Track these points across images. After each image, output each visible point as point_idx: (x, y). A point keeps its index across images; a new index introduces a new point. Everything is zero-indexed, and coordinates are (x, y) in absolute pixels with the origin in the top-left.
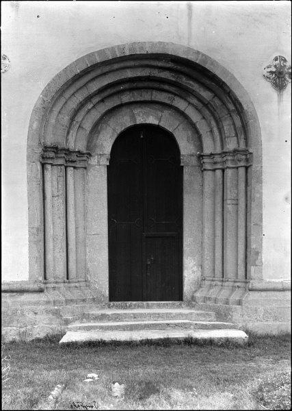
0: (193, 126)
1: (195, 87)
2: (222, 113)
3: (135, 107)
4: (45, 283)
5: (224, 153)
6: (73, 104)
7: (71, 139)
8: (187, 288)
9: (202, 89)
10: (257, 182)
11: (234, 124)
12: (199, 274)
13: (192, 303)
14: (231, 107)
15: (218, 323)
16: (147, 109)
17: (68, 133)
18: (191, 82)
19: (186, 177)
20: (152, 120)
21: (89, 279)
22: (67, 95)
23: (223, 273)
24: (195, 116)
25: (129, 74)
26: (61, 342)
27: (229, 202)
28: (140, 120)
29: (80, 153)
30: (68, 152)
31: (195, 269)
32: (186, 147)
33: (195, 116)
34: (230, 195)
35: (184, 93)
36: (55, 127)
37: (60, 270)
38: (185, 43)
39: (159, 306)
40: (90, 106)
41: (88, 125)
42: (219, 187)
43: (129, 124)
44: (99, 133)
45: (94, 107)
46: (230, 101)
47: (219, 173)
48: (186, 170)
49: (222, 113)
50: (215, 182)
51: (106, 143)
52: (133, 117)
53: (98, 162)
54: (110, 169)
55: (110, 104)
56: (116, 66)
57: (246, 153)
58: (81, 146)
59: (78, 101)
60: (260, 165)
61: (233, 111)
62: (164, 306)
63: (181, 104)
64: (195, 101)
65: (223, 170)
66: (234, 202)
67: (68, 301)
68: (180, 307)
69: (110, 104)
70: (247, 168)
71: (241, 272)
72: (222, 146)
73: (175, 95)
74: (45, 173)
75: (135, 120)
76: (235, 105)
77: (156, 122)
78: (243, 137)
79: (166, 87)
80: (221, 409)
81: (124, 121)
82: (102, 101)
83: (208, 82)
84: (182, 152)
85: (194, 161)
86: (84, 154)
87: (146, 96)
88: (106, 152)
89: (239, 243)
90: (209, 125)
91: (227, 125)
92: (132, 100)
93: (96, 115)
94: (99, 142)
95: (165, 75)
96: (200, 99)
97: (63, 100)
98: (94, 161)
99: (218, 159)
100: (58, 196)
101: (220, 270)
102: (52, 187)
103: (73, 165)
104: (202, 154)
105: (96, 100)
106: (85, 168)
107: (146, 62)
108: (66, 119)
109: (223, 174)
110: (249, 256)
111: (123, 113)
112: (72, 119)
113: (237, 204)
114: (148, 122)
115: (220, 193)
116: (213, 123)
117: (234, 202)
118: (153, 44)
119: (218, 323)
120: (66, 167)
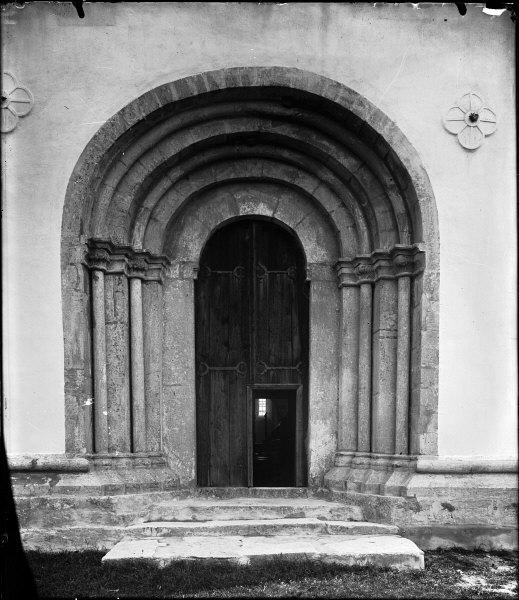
0: (326, 218)
1: (332, 150)
2: (374, 194)
3: (238, 190)
4: (134, 458)
5: (376, 255)
6: (138, 178)
7: (138, 236)
8: (314, 469)
9: (341, 153)
10: (432, 299)
11: (392, 210)
12: (332, 446)
13: (324, 490)
14: (388, 180)
15: (268, 385)
16: (254, 193)
17: (132, 226)
18: (325, 142)
19: (314, 299)
20: (263, 210)
21: (166, 451)
22: (128, 159)
23: (371, 444)
24: (330, 204)
25: (228, 128)
26: (103, 559)
27: (381, 334)
28: (245, 210)
29: (149, 257)
30: (129, 252)
31: (327, 438)
32: (314, 251)
33: (330, 204)
34: (385, 324)
35: (314, 163)
36: (108, 214)
37: (120, 432)
38: (316, 69)
39: (271, 494)
40: (166, 183)
41: (164, 216)
42: (366, 312)
43: (228, 216)
44: (182, 229)
45: (173, 186)
46: (387, 170)
47: (365, 290)
48: (314, 287)
49: (374, 194)
50: (359, 303)
51: (193, 245)
52: (234, 207)
53: (181, 274)
54: (198, 285)
55: (195, 185)
56: (206, 112)
57: (413, 252)
58: (155, 248)
59: (146, 172)
60: (435, 272)
61: (392, 187)
62: (280, 494)
63: (308, 184)
64: (330, 177)
65: (373, 286)
66: (391, 334)
67: (128, 489)
68: (304, 495)
69: (195, 185)
70: (412, 279)
71: (401, 442)
72: (372, 247)
73: (300, 168)
74: (94, 285)
75: (238, 211)
76: (395, 178)
77: (268, 213)
78: (406, 229)
79: (286, 154)
80: (205, 3)
81: (220, 211)
82: (185, 177)
83: (352, 140)
84: (309, 259)
85: (326, 273)
86: (156, 258)
87: (254, 170)
88: (192, 259)
89: (398, 397)
90: (352, 217)
91: (380, 212)
92: (232, 176)
93: (176, 199)
94: (181, 243)
95: (284, 130)
96: (338, 171)
97: (120, 170)
98: (174, 273)
99: (362, 266)
100: (115, 323)
101: (367, 438)
102: (106, 307)
103: (141, 275)
104: (340, 260)
105: (176, 174)
106: (160, 282)
107: (254, 106)
108: (127, 201)
109: (373, 292)
110: (414, 415)
111: (219, 198)
112: (138, 203)
113: (396, 338)
114: (257, 213)
115: (367, 321)
116: (358, 212)
117: (391, 334)
118: (265, 72)
119: (268, 385)
120: (130, 280)
